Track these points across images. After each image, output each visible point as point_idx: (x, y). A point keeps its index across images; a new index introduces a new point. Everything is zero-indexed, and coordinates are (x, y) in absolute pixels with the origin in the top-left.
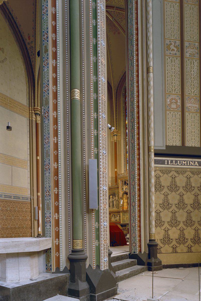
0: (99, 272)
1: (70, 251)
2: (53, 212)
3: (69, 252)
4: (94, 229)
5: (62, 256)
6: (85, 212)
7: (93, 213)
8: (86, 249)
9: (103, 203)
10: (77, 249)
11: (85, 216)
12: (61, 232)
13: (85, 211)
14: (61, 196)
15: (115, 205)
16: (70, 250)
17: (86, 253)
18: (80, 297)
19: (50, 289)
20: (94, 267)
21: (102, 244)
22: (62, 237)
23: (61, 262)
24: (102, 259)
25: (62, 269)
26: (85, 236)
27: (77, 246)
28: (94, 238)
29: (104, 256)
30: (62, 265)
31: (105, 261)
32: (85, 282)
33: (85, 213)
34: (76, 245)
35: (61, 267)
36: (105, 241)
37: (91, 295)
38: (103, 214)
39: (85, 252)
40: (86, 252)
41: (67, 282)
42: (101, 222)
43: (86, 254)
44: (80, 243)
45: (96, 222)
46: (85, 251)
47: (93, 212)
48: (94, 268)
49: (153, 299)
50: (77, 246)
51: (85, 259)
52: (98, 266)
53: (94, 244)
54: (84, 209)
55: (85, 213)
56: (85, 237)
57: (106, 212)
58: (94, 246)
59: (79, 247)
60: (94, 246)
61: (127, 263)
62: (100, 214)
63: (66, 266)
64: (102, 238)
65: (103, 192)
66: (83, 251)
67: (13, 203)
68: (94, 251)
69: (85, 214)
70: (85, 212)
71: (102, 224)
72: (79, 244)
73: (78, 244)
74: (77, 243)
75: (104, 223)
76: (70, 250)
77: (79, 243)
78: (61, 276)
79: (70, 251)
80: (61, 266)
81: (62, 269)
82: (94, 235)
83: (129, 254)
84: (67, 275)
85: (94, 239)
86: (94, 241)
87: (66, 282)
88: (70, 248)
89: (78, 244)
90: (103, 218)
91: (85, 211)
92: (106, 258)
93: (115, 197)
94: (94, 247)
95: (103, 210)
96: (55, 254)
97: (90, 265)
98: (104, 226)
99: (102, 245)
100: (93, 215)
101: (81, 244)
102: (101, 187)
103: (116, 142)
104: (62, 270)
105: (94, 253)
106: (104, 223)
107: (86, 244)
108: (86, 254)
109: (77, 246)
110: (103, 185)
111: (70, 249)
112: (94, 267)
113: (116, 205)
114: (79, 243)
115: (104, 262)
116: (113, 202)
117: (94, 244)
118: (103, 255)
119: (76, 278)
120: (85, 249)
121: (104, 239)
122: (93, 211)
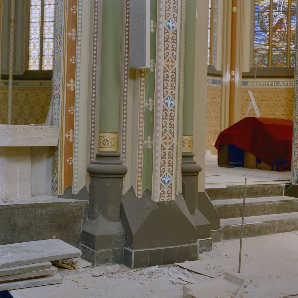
0: (149, 204)
1: (92, 155)
2: (64, 76)
3: (91, 158)
4: (143, 113)
5: (77, 165)
6: (126, 77)
7: (143, 79)
8: (125, 153)
9: (165, 58)
10: (106, 152)
11: (126, 85)
12: (78, 116)
13: (127, 75)
14: (80, 45)
16: (93, 153)
17: (125, 162)
18: (95, 250)
19: (37, 224)
20: (139, 193)
21: (158, 145)
22: (78, 125)
23: (75, 176)
24: (157, 178)
25: (76, 190)
26: (124, 127)
27: (103, 146)
28: (142, 131)
29: (161, 171)
30: (77, 183)
31: (164, 182)
32: (119, 221)
33: (127, 79)
34: (102, 144)
35: (74, 187)
36: (165, 138)
37: (125, 250)
38: (164, 80)
39: (122, 159)
40: (124, 160)
41: (79, 217)
42: (158, 98)
43: (124, 164)
44: (110, 141)
45: (149, 98)
46: (123, 158)
47: (141, 77)
48: (138, 195)
49: (238, 275)
50: (103, 146)
51: (121, 175)
52: (148, 192)
53: (142, 145)
54: (125, 70)
55: (125, 79)
56: (124, 129)
57: (173, 77)
58: (141, 147)
59: (108, 149)
60: (141, 147)
61: (268, 202)
62: (157, 81)
63: (85, 186)
64: (158, 131)
65: (165, 33)
66: (118, 157)
67: (214, 90)
68: (141, 158)
69: (126, 81)
70: (126, 77)
71: (159, 101)
72: (107, 143)
73: (106, 142)
74: (104, 140)
75: (167, 99)
76: (93, 153)
77: (108, 139)
78: (66, 203)
79: (92, 155)
80: (75, 185)
81: (76, 190)
82: (141, 125)
83: (287, 186)
84: (83, 202)
85: (141, 134)
86: (141, 138)
87: (78, 216)
88: (93, 149)
89: (106, 141)
90: (164, 88)
91: (127, 75)
92: (167, 178)
94: (142, 150)
95: (164, 72)
96: (65, 159)
97: (132, 188)
98: (164, 107)
99: (159, 148)
100: (141, 82)
101: (113, 142)
102: (160, 23)
104: (75, 193)
105: (141, 163)
106: (166, 101)
107: (124, 142)
108: (124, 164)
109: (104, 145)
110: (166, 19)
111: (92, 151)
112: (139, 192)
114: (107, 140)
115: (161, 185)
117: (142, 145)
118: (158, 168)
119: (96, 210)
120: (123, 153)
121: (163, 135)
122: (143, 75)
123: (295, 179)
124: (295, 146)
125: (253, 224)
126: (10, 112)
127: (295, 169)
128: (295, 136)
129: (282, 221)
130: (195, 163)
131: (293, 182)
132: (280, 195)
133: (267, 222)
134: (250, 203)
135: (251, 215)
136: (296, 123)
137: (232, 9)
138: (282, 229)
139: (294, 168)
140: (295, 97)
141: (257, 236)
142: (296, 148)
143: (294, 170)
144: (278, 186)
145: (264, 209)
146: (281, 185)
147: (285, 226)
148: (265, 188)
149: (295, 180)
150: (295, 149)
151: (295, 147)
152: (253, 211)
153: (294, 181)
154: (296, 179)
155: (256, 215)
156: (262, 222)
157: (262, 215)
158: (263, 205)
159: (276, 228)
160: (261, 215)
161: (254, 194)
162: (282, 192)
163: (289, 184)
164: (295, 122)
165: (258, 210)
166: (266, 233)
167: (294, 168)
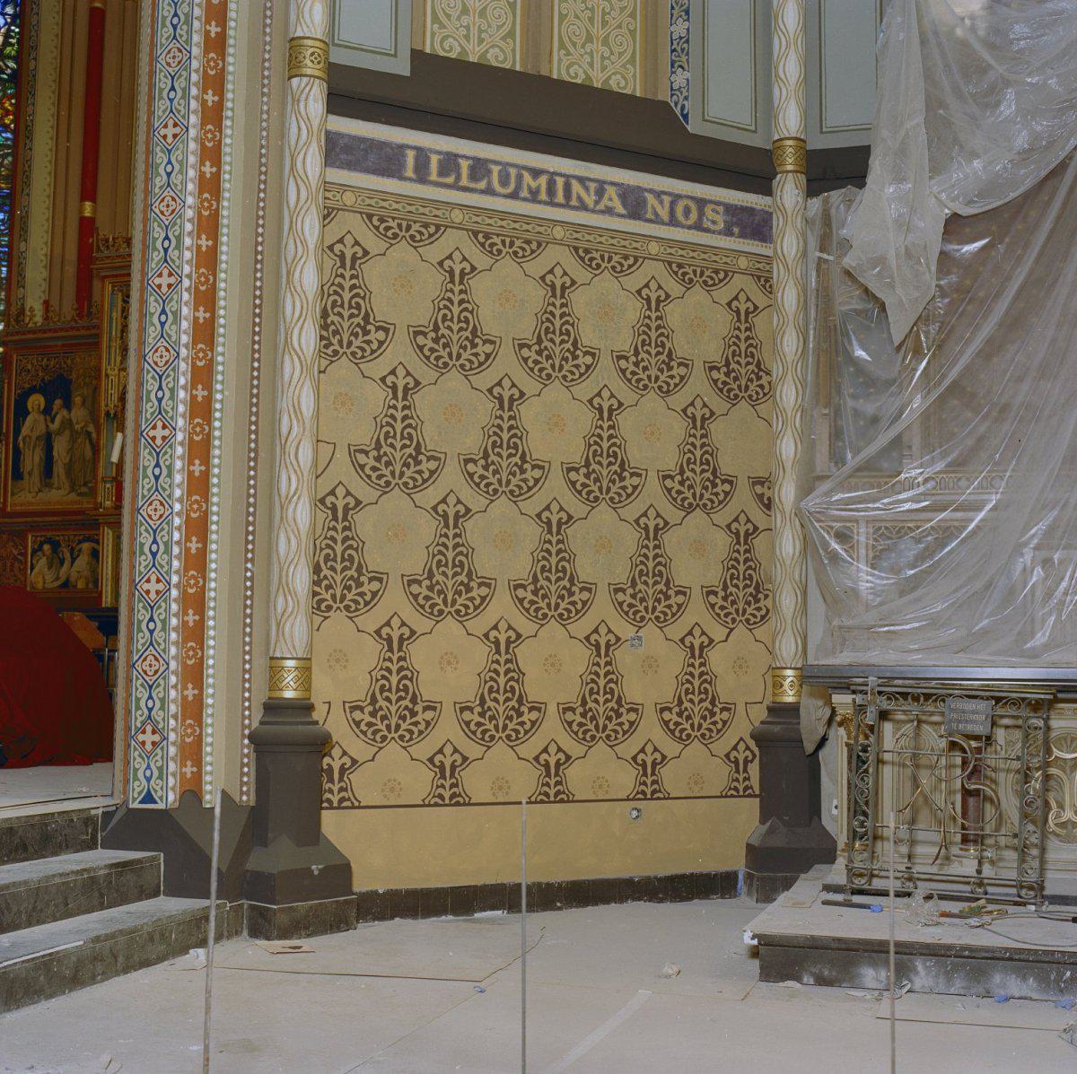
15: (59, 469)
93: (68, 405)
103: (83, 198)
113: (69, 469)
116: (48, 440)
123: (137, 790)
124: (137, 679)
125: (58, 952)
126: (782, 379)
127: (140, 756)
128: (140, 647)
129: (134, 931)
130: (316, 723)
131: (134, 799)
132: (91, 849)
133: (97, 939)
134: (26, 882)
135: (30, 925)
136: (141, 605)
137: (81, 210)
138: (136, 958)
139: (137, 753)
140: (140, 517)
141: (70, 991)
142: (142, 685)
143: (135, 759)
144: (84, 815)
145: (66, 899)
146: (93, 812)
147: (143, 947)
148: (46, 825)
149: (140, 793)
150: (141, 689)
151: (139, 682)
152: (34, 909)
153: (136, 796)
154: (142, 791)
155: (44, 923)
156: (82, 943)
157: (62, 918)
158: (63, 883)
159: (121, 959)
160: (55, 920)
161: (16, 850)
162: (94, 837)
163: (114, 808)
164: (140, 601)
165: (47, 905)
166: (93, 980)
167: (137, 753)
